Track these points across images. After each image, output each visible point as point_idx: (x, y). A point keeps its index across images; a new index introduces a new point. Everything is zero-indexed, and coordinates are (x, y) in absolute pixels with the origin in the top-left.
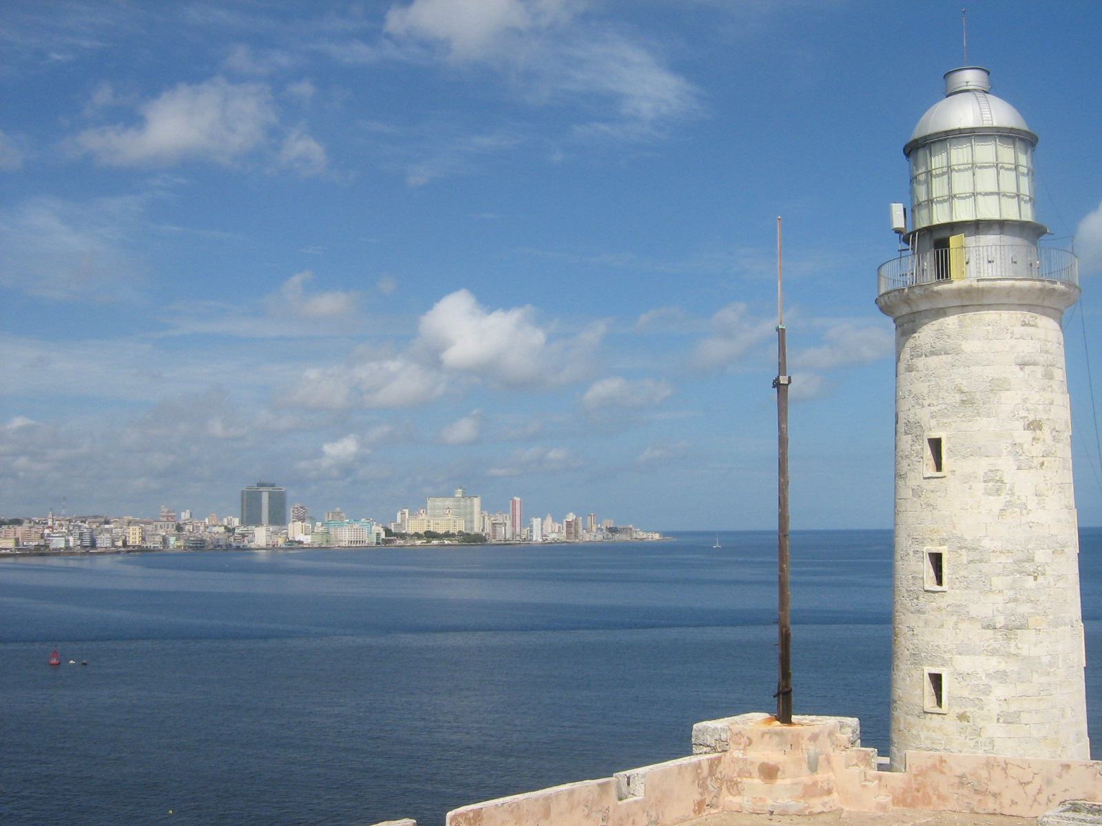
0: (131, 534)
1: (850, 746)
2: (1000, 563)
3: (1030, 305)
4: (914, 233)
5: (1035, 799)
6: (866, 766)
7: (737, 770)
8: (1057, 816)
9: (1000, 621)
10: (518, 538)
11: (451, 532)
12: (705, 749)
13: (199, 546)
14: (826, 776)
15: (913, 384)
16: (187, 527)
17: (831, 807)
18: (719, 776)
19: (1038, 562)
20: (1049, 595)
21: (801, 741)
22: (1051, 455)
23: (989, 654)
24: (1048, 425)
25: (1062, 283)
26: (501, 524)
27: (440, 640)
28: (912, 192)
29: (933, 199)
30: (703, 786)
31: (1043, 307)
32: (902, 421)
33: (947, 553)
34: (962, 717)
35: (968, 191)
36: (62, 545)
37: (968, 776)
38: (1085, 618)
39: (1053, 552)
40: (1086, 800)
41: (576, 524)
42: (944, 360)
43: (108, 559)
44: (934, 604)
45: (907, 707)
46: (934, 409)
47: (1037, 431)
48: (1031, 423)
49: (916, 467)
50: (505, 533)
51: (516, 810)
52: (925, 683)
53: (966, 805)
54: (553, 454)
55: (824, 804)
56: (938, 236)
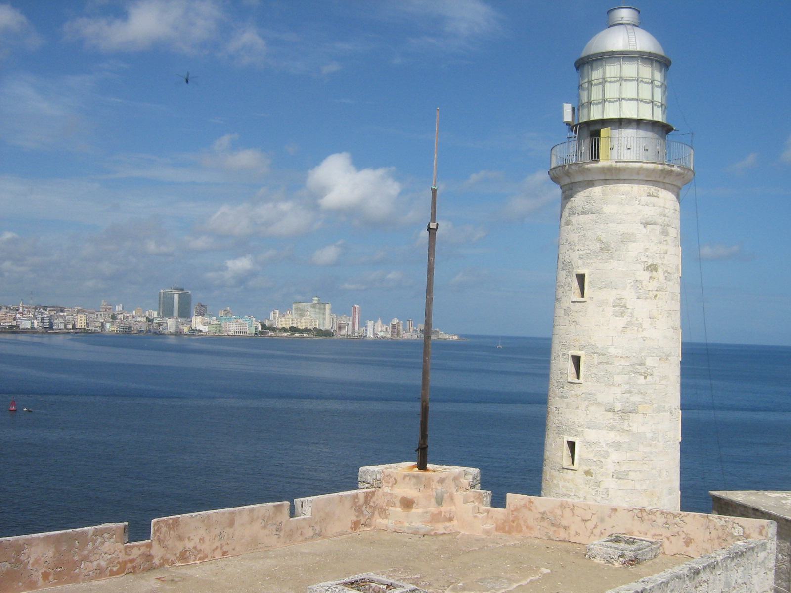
0: (78, 320)
1: (469, 488)
2: (620, 365)
3: (654, 181)
4: (576, 125)
5: (592, 532)
6: (480, 502)
7: (386, 500)
8: (600, 544)
9: (618, 406)
10: (356, 334)
11: (309, 328)
12: (367, 485)
13: (127, 331)
14: (449, 508)
15: (569, 234)
16: (119, 317)
17: (451, 530)
18: (372, 504)
19: (648, 366)
20: (655, 390)
21: (432, 483)
22: (663, 290)
23: (609, 429)
24: (662, 268)
25: (678, 167)
26: (345, 323)
27: (307, 405)
28: (579, 96)
29: (591, 102)
30: (359, 511)
31: (664, 183)
32: (561, 260)
33: (584, 356)
34: (588, 473)
35: (615, 97)
36: (29, 326)
37: (548, 514)
38: (683, 407)
39: (660, 359)
40: (626, 534)
41: (399, 325)
42: (591, 218)
43: (61, 337)
44: (573, 392)
45: (552, 464)
46: (581, 253)
47: (654, 272)
48: (650, 266)
49: (567, 294)
50: (347, 330)
51: (206, 520)
52: (564, 447)
53: (545, 533)
54: (390, 276)
55: (445, 528)
56: (594, 128)
